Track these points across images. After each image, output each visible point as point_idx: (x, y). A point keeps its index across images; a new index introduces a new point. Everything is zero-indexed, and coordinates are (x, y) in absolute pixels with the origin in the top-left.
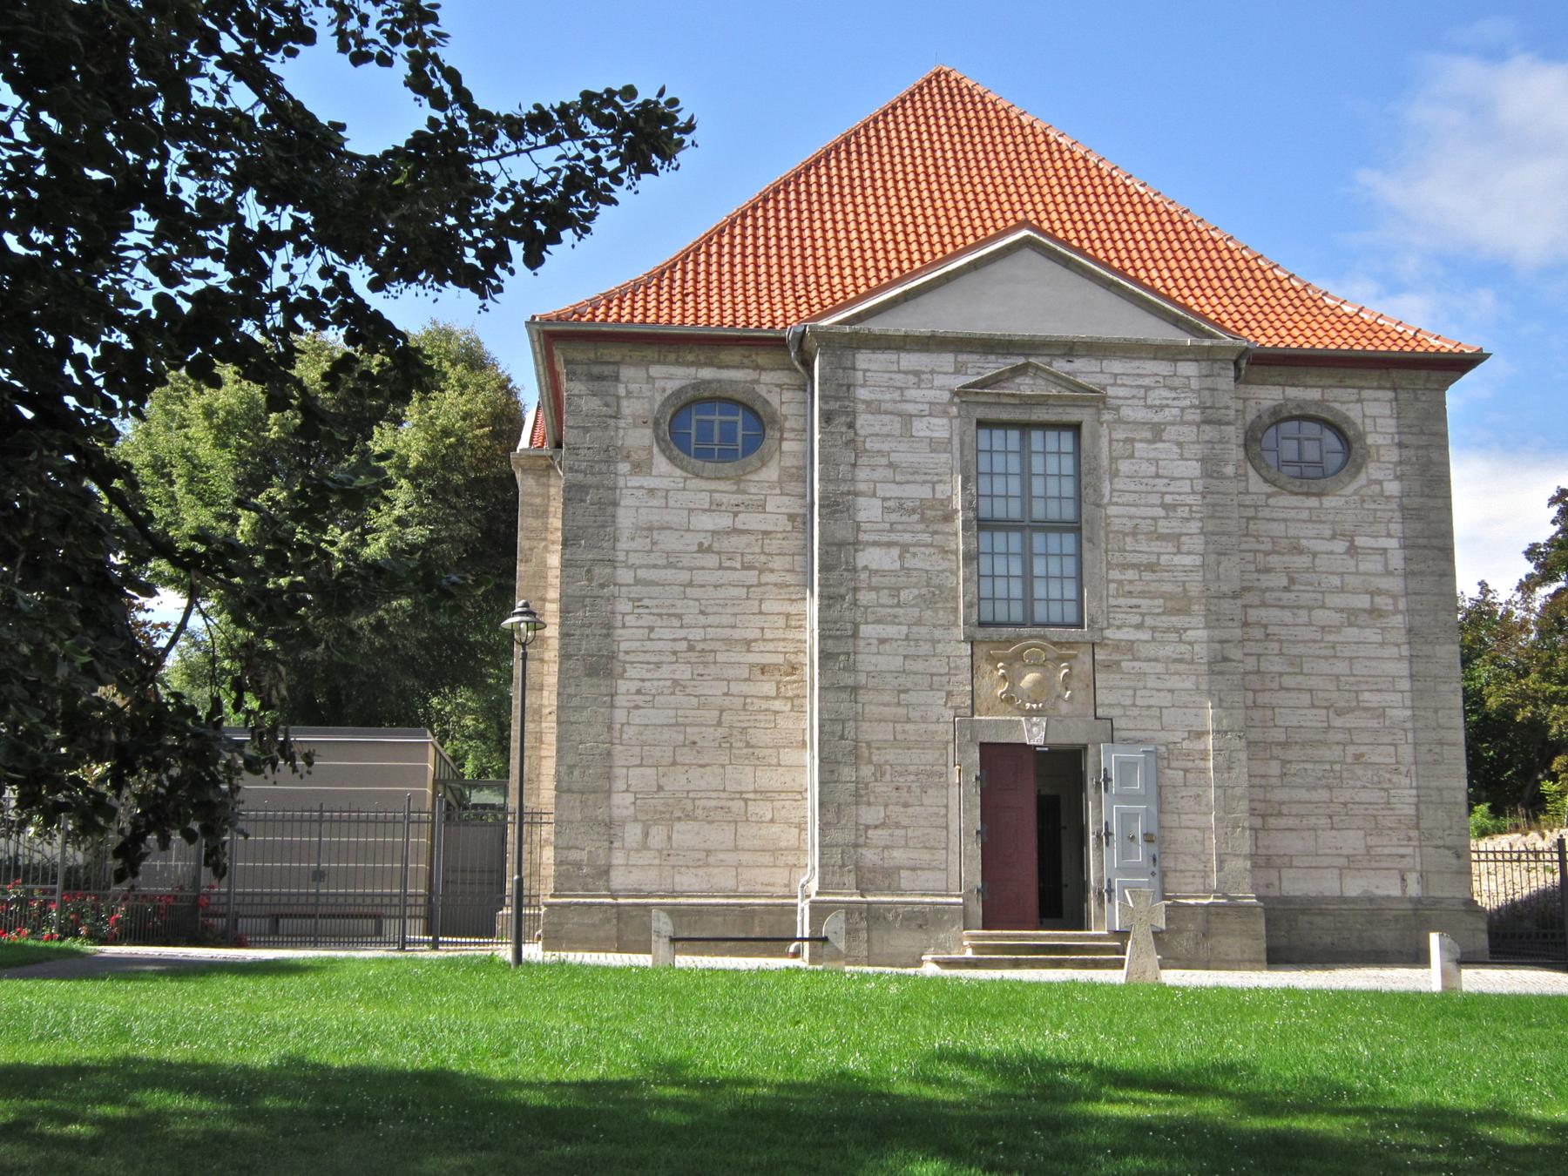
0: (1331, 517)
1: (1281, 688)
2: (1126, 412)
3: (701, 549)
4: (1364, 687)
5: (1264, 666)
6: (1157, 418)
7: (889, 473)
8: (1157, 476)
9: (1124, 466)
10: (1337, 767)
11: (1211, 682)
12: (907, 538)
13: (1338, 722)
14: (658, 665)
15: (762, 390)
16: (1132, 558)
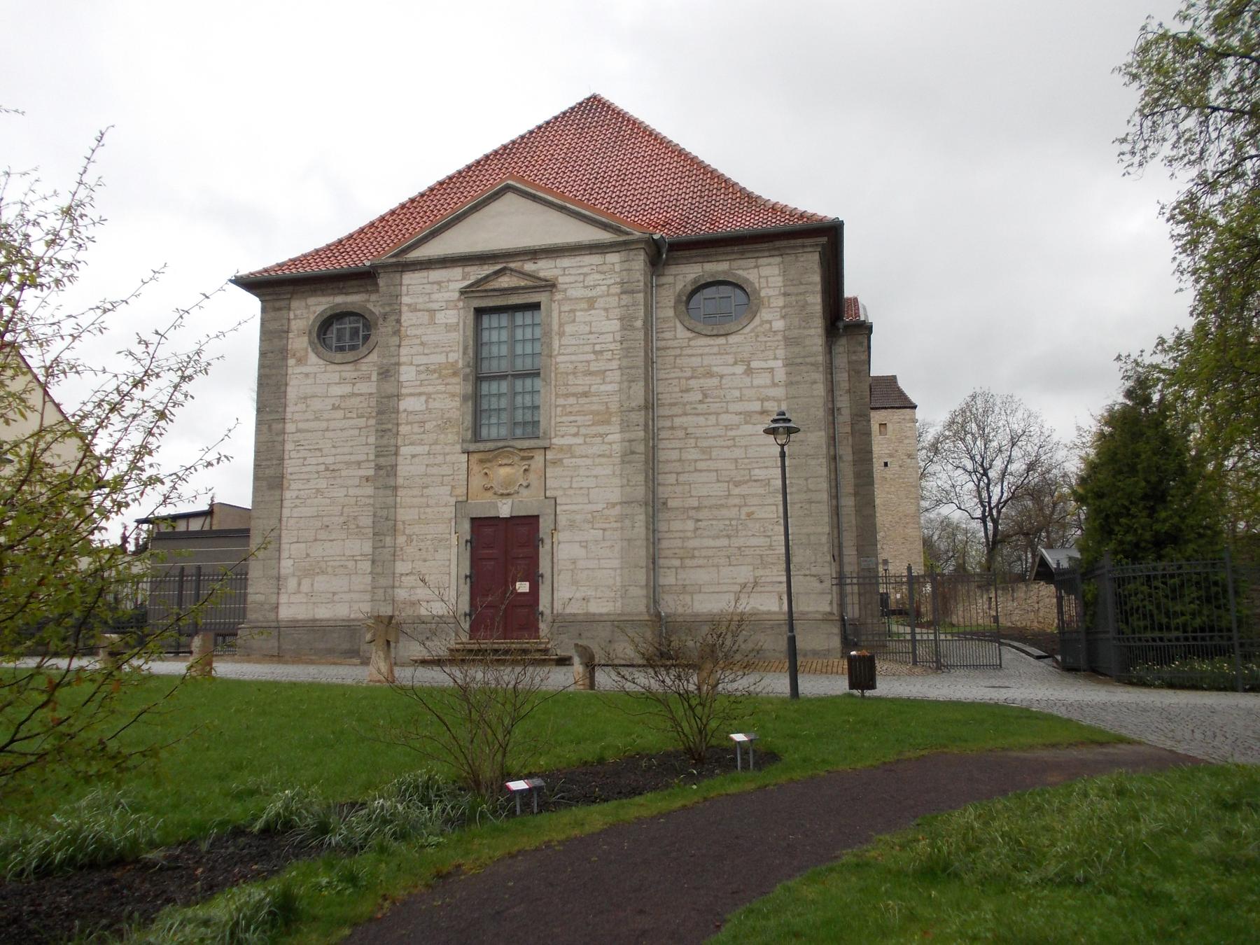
0: (733, 350)
1: (696, 470)
2: (572, 293)
3: (335, 408)
4: (755, 465)
5: (684, 456)
6: (590, 294)
7: (420, 349)
8: (591, 333)
9: (569, 329)
10: (734, 523)
11: (622, 470)
12: (430, 389)
13: (736, 491)
14: (308, 480)
15: (370, 306)
16: (572, 390)
